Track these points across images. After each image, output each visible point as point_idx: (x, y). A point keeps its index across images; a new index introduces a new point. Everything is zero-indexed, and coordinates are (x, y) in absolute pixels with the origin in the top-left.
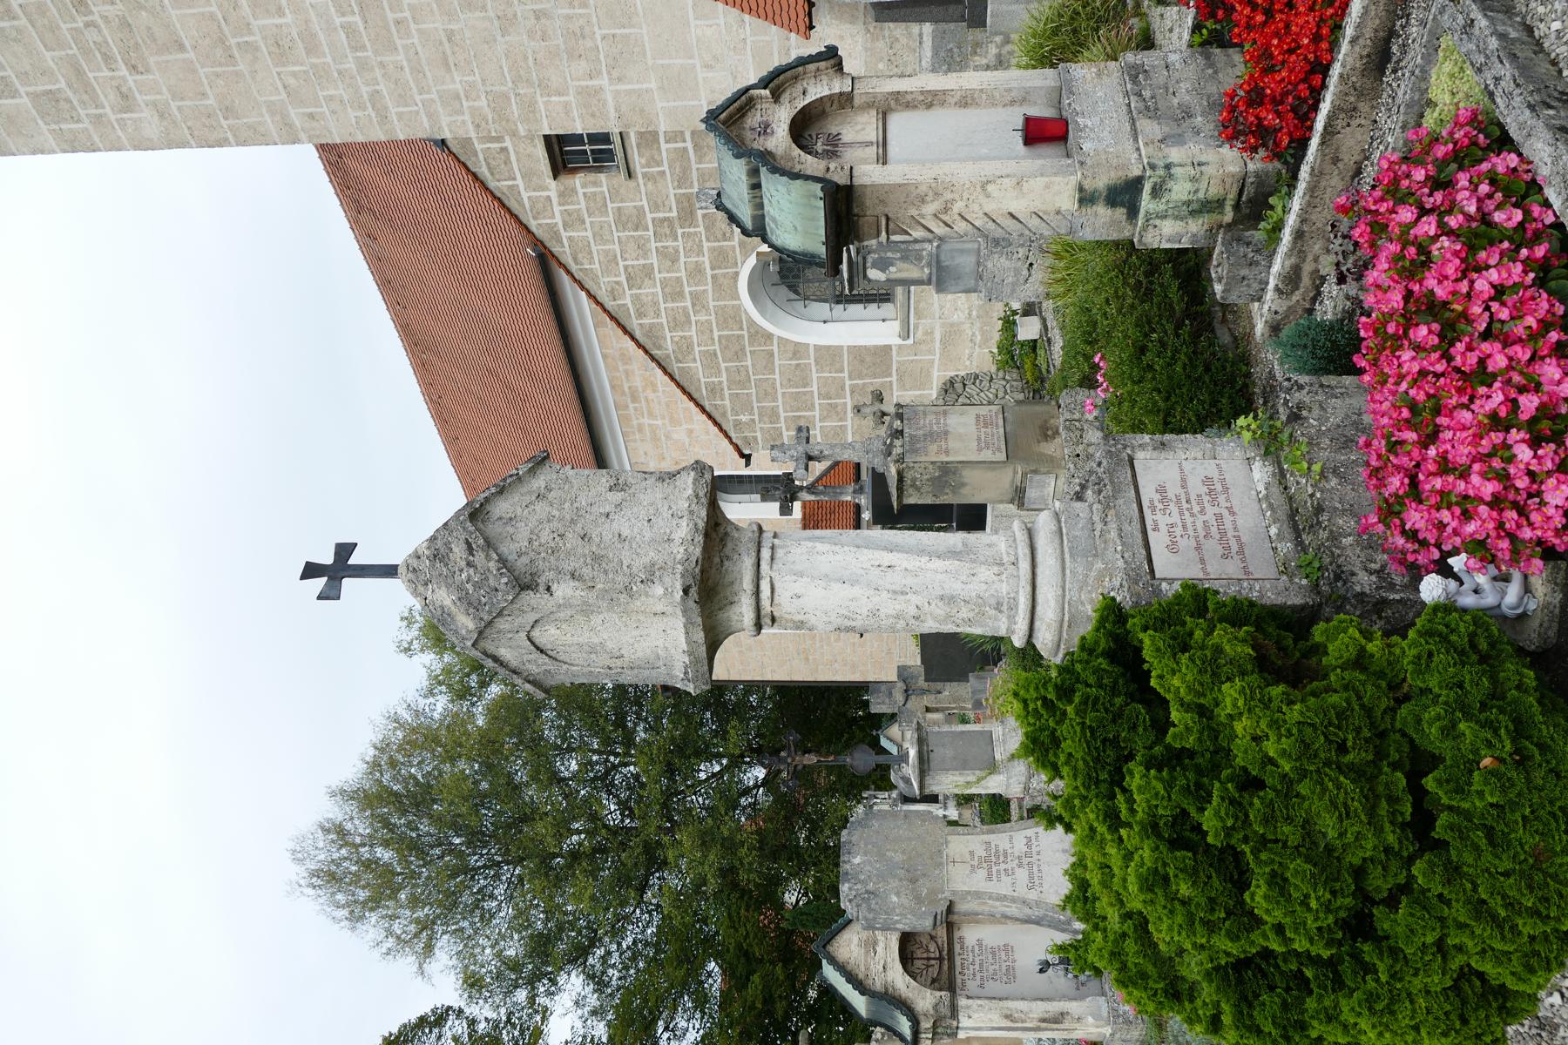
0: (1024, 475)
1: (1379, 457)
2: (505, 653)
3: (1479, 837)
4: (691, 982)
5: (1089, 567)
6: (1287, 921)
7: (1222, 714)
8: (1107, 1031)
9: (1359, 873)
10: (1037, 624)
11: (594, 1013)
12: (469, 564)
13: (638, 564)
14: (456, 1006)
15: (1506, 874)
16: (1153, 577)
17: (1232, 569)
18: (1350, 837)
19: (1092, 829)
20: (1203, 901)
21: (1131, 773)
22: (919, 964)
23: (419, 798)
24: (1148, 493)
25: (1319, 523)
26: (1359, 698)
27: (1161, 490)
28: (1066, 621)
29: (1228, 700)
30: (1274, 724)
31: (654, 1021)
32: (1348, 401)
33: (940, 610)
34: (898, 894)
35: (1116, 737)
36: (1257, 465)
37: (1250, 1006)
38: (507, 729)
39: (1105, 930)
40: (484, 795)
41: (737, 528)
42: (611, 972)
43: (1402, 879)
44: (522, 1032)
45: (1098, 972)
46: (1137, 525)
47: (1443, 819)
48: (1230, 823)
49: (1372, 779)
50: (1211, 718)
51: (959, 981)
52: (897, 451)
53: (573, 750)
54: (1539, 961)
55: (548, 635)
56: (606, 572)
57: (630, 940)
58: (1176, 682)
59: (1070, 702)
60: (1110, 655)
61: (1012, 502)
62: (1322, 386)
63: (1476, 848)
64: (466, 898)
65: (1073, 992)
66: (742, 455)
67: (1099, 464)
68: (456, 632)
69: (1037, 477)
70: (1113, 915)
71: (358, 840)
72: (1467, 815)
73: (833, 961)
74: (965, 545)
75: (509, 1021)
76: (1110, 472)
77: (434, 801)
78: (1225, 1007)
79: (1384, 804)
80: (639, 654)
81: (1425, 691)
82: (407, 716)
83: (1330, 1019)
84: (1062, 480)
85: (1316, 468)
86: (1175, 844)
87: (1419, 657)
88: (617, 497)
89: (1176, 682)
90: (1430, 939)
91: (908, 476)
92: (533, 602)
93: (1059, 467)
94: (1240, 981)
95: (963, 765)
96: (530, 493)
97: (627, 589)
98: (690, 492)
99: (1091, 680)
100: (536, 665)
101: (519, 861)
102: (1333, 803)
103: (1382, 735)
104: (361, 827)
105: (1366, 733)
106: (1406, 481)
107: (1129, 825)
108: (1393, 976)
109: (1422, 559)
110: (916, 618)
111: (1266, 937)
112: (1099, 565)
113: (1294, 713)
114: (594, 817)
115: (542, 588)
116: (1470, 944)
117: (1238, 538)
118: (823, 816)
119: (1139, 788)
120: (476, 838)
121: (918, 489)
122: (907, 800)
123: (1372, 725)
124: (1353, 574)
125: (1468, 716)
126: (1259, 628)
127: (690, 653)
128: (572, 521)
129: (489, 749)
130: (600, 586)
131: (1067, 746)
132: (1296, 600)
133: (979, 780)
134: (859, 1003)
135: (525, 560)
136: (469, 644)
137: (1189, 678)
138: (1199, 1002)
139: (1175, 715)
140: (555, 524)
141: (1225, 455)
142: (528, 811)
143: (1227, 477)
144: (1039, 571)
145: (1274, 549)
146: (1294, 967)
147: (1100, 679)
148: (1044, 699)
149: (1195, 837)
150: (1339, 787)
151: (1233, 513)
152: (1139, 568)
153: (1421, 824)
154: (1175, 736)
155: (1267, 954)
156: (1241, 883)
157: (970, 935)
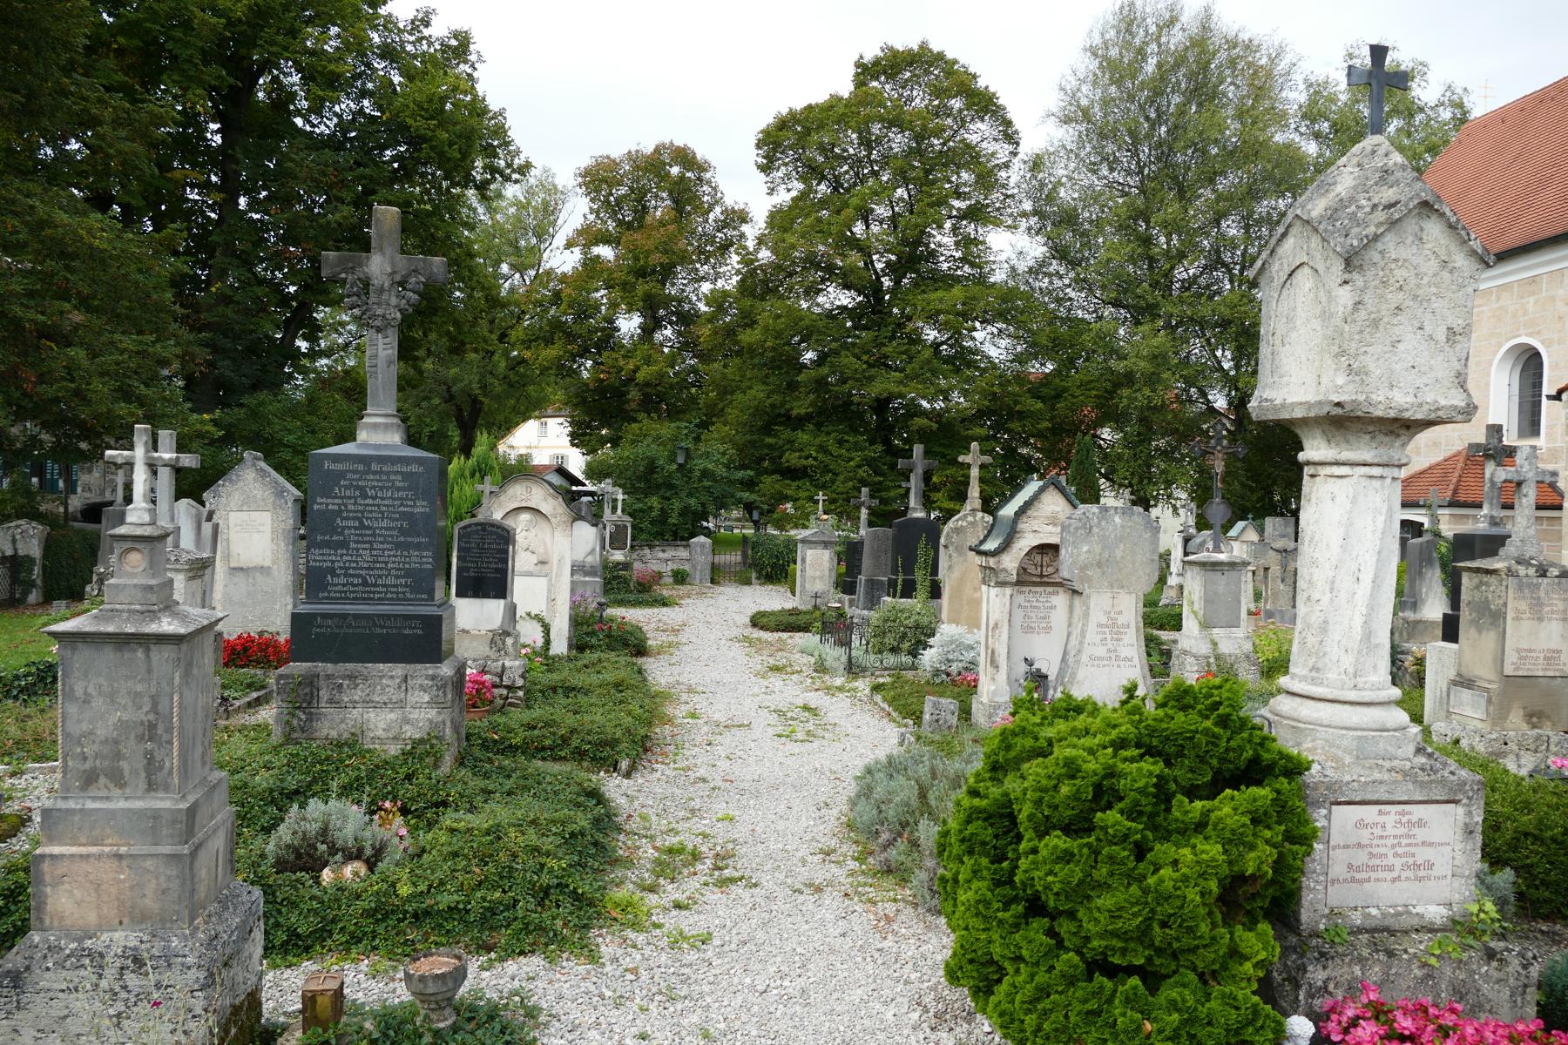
0: (1487, 690)
1: (1437, 1017)
2: (1290, 242)
3: (1092, 1005)
4: (1036, 350)
5: (1347, 751)
6: (1040, 857)
7: (1197, 840)
8: (985, 699)
9: (1072, 915)
10: (1298, 700)
11: (1013, 269)
12: (1375, 206)
13: (1369, 362)
14: (1020, 149)
15: (1066, 1017)
16: (1333, 803)
17: (1338, 870)
18: (1097, 915)
19: (1115, 726)
20: (1056, 801)
21: (1155, 763)
22: (1038, 558)
23: (1203, 91)
24: (1418, 811)
25: (1377, 951)
26: (1205, 946)
27: (1421, 823)
28: (1299, 728)
29: (1207, 847)
30: (1185, 879)
31: (1006, 321)
32: (1507, 1006)
33: (1316, 619)
34: (1089, 551)
35: (1183, 756)
36: (1443, 911)
37: (985, 820)
38: (1269, 167)
39: (1041, 724)
40: (1205, 152)
41: (1404, 445)
42: (1046, 280)
43: (1067, 944)
44: (998, 209)
45: (1013, 714)
46: (1385, 797)
47: (1108, 984)
48: (1111, 831)
49: (1140, 940)
50: (1196, 830)
51: (1026, 589)
52: (1522, 570)
53: (1247, 232)
54: (1007, 1022)
55: (1304, 279)
56: (1361, 332)
57: (1073, 295)
58: (1227, 810)
59: (1216, 724)
60: (1255, 761)
61: (1459, 675)
62: (1526, 986)
63: (1085, 1001)
64: (1110, 148)
65: (1013, 677)
66: (1560, 392)
67: (1452, 773)
68: (1310, 199)
69: (1483, 702)
70: (1050, 732)
71: (1163, 39)
72: (1110, 1001)
73: (1042, 490)
74: (1377, 646)
75: (1008, 196)
76: (1443, 782)
77: (1200, 105)
78: (985, 803)
79: (1120, 944)
80: (1285, 361)
81: (1208, 997)
82: (1283, 65)
83: (974, 872)
84: (1480, 725)
85: (1433, 961)
86: (1098, 788)
87: (1235, 999)
88: (1441, 335)
89: (1227, 810)
90: (1024, 952)
91: (1492, 579)
92: (1334, 269)
93: (1494, 724)
94: (1002, 816)
95: (1208, 601)
96: (1449, 254)
97: (1343, 353)
98: (1443, 402)
99: (1233, 744)
100: (1278, 270)
101: (1143, 192)
102: (1121, 909)
103: (1175, 956)
104: (1176, 39)
105: (1176, 945)
106: (1407, 1033)
107: (1115, 756)
108: (1001, 922)
109: (1332, 1025)
110: (1309, 598)
111: (1030, 840)
112: (1348, 760)
113: (1193, 895)
114: (1182, 256)
115: (1347, 276)
116: (1020, 979)
117: (1369, 880)
118: (1178, 461)
119: (1140, 769)
120: (1164, 152)
121: (1477, 587)
122: (1187, 541)
123: (1183, 951)
124: (1325, 968)
125: (1184, 1023)
126: (1272, 882)
127: (1283, 405)
128: (1415, 297)
129: (1249, 151)
130: (1347, 327)
131: (1180, 717)
132: (1305, 916)
133: (1194, 613)
134: (1009, 510)
135: (1376, 257)
136: (1298, 212)
137: (1229, 821)
138: (989, 784)
139: (1198, 804)
140: (1413, 281)
141: (1456, 884)
142: (1188, 195)
143: (1433, 883)
144: (1347, 707)
145: (1356, 908)
146: (1010, 855)
147: (1234, 750)
148: (1220, 703)
149: (1103, 802)
150: (1135, 915)
151: (1394, 880)
152: (1342, 794)
153: (1099, 966)
154: (1181, 802)
155: (1019, 838)
156: (1067, 830)
157: (1060, 600)
